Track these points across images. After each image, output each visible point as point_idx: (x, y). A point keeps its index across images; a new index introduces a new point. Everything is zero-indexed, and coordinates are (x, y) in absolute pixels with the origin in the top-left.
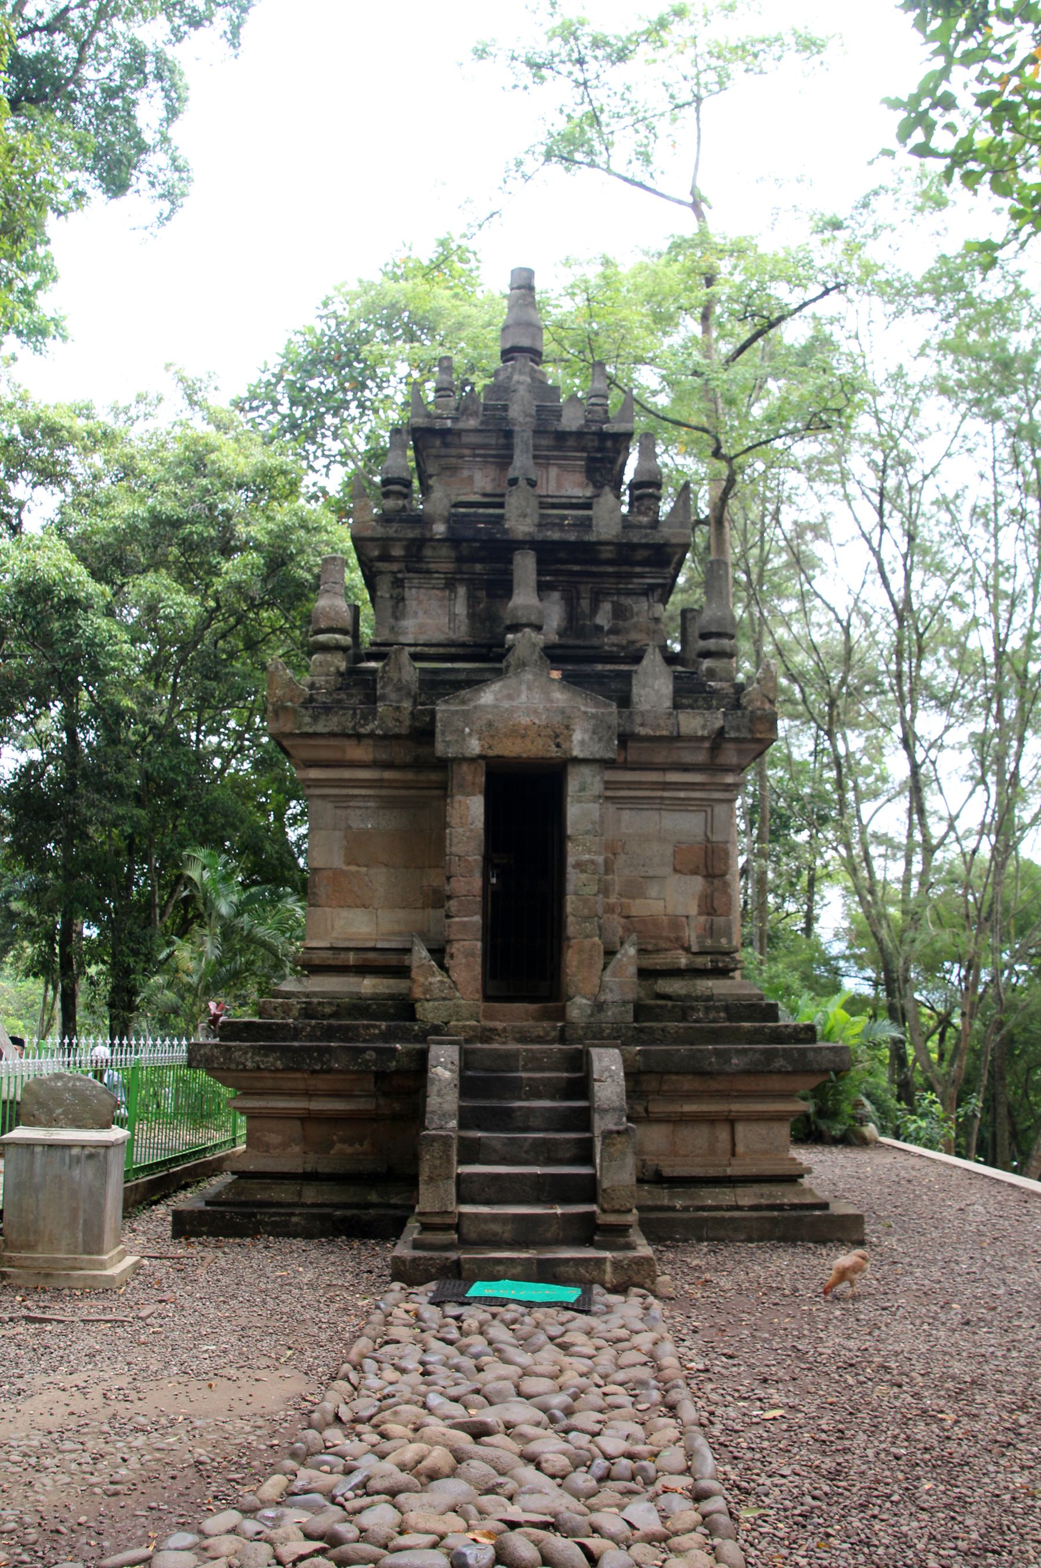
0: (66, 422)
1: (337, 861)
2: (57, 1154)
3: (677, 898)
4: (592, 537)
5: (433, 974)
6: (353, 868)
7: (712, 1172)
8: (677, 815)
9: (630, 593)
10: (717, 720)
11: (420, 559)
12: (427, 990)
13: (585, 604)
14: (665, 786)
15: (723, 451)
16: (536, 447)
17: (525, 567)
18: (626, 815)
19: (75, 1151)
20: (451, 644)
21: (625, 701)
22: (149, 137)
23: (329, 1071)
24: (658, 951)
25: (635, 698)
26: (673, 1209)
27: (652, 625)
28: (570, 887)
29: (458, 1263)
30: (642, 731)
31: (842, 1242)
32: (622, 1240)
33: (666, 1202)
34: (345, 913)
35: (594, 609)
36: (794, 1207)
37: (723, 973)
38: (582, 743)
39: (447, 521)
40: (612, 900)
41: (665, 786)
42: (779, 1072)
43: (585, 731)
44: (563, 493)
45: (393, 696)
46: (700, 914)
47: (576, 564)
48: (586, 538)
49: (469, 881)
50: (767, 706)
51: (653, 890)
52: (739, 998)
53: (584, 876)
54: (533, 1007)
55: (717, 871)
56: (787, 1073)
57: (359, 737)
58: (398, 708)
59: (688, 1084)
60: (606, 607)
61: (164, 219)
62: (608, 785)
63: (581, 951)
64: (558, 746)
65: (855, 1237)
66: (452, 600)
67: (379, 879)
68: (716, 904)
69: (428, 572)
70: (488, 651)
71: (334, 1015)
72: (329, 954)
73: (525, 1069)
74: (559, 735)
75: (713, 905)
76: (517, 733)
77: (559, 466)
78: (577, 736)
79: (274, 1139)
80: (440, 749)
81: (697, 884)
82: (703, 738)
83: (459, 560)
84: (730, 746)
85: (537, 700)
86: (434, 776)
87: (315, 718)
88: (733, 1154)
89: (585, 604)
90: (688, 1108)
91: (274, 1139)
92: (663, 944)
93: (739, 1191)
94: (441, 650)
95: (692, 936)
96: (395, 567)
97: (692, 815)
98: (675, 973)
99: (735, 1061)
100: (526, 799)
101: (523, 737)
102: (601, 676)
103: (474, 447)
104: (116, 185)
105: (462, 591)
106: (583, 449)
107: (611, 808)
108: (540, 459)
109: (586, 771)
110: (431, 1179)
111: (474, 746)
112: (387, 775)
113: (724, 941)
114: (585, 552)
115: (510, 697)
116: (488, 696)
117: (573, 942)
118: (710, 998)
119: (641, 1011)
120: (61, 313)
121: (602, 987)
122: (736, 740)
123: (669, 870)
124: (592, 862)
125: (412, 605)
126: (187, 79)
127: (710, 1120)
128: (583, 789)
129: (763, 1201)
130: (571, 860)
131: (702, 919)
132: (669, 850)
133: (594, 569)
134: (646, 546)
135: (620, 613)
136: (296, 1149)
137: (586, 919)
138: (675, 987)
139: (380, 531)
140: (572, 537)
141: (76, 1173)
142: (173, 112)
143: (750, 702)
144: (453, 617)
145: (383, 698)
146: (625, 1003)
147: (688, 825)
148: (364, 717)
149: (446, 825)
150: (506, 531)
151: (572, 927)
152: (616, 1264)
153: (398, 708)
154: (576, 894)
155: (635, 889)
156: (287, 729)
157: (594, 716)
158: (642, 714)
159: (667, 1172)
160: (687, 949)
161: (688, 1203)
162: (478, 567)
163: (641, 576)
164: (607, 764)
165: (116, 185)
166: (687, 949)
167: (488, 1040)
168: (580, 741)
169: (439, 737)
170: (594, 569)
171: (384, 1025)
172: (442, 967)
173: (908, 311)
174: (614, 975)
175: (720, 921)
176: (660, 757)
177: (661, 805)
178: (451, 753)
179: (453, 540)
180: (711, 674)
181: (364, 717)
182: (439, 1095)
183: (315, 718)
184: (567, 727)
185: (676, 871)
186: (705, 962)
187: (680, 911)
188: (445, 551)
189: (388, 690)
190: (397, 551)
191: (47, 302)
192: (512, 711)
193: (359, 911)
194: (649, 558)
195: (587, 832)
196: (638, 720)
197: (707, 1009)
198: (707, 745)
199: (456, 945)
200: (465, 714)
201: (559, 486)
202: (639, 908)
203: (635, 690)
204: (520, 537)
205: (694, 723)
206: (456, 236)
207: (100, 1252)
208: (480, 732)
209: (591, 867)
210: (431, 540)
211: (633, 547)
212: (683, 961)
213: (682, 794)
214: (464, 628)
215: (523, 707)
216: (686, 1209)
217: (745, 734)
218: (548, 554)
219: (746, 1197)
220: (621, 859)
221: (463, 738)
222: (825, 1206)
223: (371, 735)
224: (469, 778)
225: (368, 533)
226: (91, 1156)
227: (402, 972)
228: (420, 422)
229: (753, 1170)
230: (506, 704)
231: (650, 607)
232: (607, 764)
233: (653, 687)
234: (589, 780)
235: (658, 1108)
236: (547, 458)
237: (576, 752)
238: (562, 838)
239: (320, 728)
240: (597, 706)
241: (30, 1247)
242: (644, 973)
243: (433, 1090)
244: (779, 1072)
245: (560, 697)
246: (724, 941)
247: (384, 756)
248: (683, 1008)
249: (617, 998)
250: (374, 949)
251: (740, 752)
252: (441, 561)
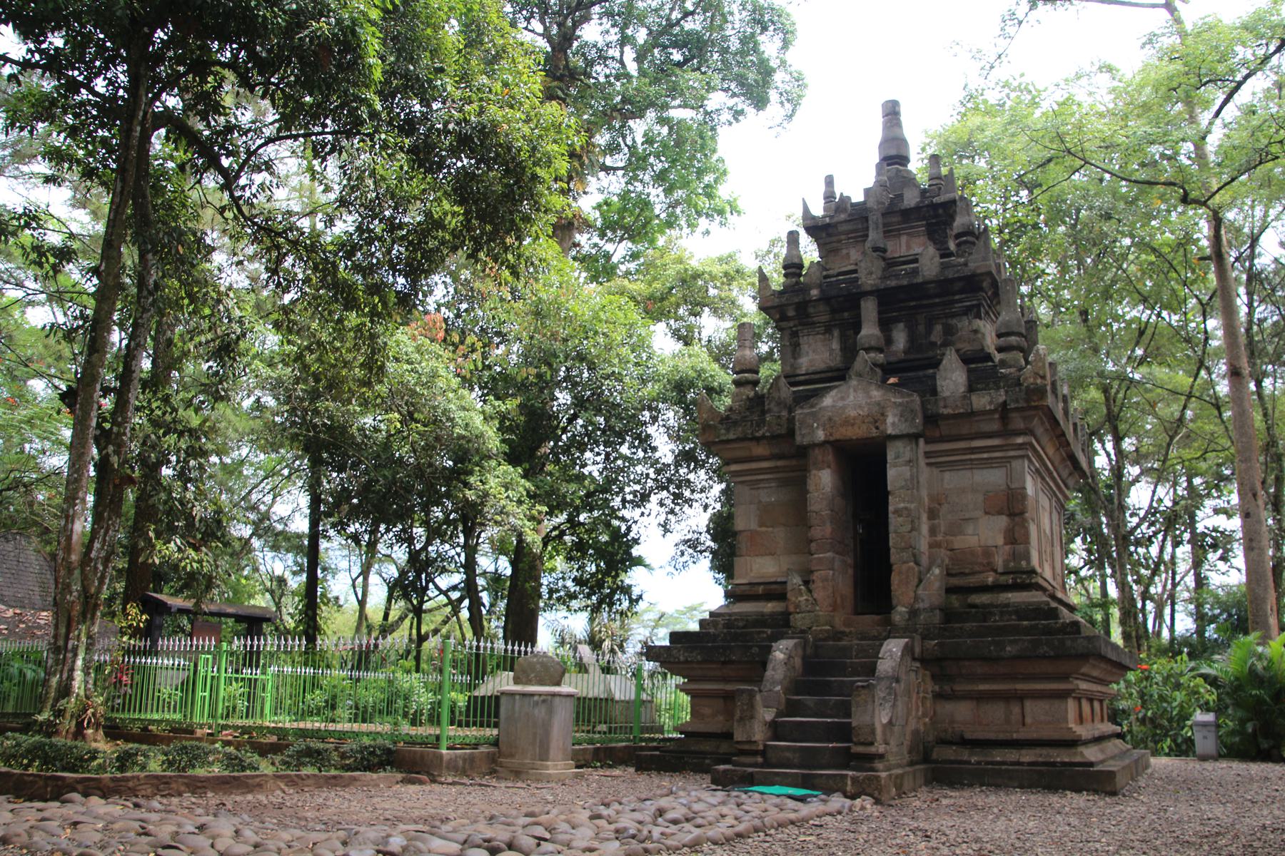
0: (707, 269)
1: (754, 525)
2: (527, 700)
3: (987, 533)
4: (920, 280)
5: (801, 595)
6: (764, 529)
7: (1001, 736)
8: (985, 471)
9: (954, 315)
10: (1001, 396)
11: (808, 316)
12: (797, 606)
13: (921, 328)
14: (1050, 474)
15: (1193, 195)
16: (885, 225)
17: (869, 309)
18: (947, 475)
19: (536, 698)
20: (830, 370)
21: (932, 390)
22: (774, 63)
23: (732, 662)
24: (973, 573)
25: (939, 389)
26: (969, 763)
27: (972, 336)
28: (891, 528)
29: (751, 774)
30: (946, 411)
31: (1096, 792)
32: (868, 765)
33: (965, 758)
34: (759, 560)
35: (929, 331)
36: (1064, 764)
38: (893, 424)
39: (820, 286)
40: (939, 538)
41: (1050, 474)
42: (1044, 657)
43: (895, 415)
44: (912, 252)
45: (776, 409)
46: (1006, 544)
48: (915, 281)
50: (1039, 381)
51: (970, 529)
52: (1030, 604)
53: (900, 519)
54: (876, 618)
55: (1017, 511)
56: (1050, 657)
57: (757, 440)
58: (779, 417)
59: (979, 668)
60: (938, 328)
61: (790, 117)
63: (900, 573)
64: (877, 428)
65: (1108, 789)
68: (1016, 535)
69: (814, 323)
71: (744, 627)
72: (747, 588)
73: (856, 657)
74: (877, 419)
75: (1016, 537)
76: (848, 422)
77: (908, 234)
78: (890, 420)
79: (707, 711)
81: (1003, 521)
82: (991, 412)
83: (833, 311)
84: (1014, 415)
87: (728, 430)
88: (1024, 724)
89: (921, 328)
90: (982, 687)
91: (707, 711)
92: (977, 568)
93: (1024, 752)
94: (823, 375)
95: (999, 562)
96: (791, 324)
97: (996, 471)
98: (985, 589)
99: (1008, 648)
100: (863, 465)
101: (853, 425)
103: (847, 233)
104: (760, 102)
105: (836, 333)
106: (924, 218)
107: (936, 471)
110: (741, 719)
111: (821, 435)
112: (780, 463)
113: (1024, 563)
115: (842, 399)
116: (828, 401)
117: (894, 567)
118: (1007, 605)
119: (949, 615)
120: (735, 196)
121: (916, 598)
122: (1017, 409)
123: (979, 513)
124: (906, 508)
125: (805, 347)
126: (794, 18)
127: (1007, 697)
128: (897, 457)
129: (1040, 759)
130: (891, 508)
131: (1007, 548)
132: (980, 498)
133: (925, 302)
134: (960, 279)
136: (721, 718)
137: (903, 549)
138: (984, 599)
140: (905, 282)
141: (536, 711)
142: (786, 44)
143: (1026, 379)
145: (769, 411)
146: (932, 609)
147: (994, 478)
148: (758, 425)
149: (807, 492)
150: (859, 286)
151: (894, 557)
152: (854, 780)
153: (779, 417)
154: (896, 532)
155: (956, 529)
156: (710, 439)
157: (900, 404)
158: (945, 399)
159: (968, 736)
160: (995, 571)
161: (982, 759)
162: (846, 314)
163: (960, 301)
165: (760, 102)
166: (995, 571)
167: (840, 639)
168: (892, 424)
169: (797, 433)
170: (925, 302)
171: (769, 631)
172: (810, 591)
174: (925, 589)
175: (1020, 548)
176: (965, 430)
178: (806, 441)
179: (825, 299)
181: (758, 425)
182: (774, 669)
183: (728, 430)
184: (883, 414)
185: (986, 513)
187: (990, 543)
188: (822, 307)
189: (772, 405)
190: (791, 313)
191: (723, 192)
192: (844, 408)
193: (768, 558)
195: (902, 487)
196: (942, 404)
197: (1002, 613)
198: (997, 416)
199: (816, 574)
200: (814, 415)
201: (909, 247)
202: (959, 542)
203: (938, 383)
204: (869, 289)
205: (981, 401)
206: (975, 83)
207: (547, 760)
208: (824, 425)
209: (905, 512)
210: (811, 301)
211: (952, 281)
213: (985, 456)
214: (838, 358)
216: (979, 763)
217: (1022, 404)
219: (1027, 756)
220: (945, 508)
221: (813, 430)
222: (1091, 764)
223: (763, 437)
224: (820, 457)
225: (769, 304)
226: (544, 701)
227: (782, 597)
229: (1035, 736)
230: (840, 404)
231: (970, 323)
232: (913, 438)
234: (901, 450)
235: (960, 687)
236: (899, 230)
239: (731, 436)
240: (902, 397)
241: (512, 756)
243: (770, 666)
244: (1044, 657)
245: (876, 394)
246: (1024, 563)
247: (776, 451)
248: (984, 612)
249: (927, 605)
250: (776, 583)
251: (1024, 418)
252: (821, 314)
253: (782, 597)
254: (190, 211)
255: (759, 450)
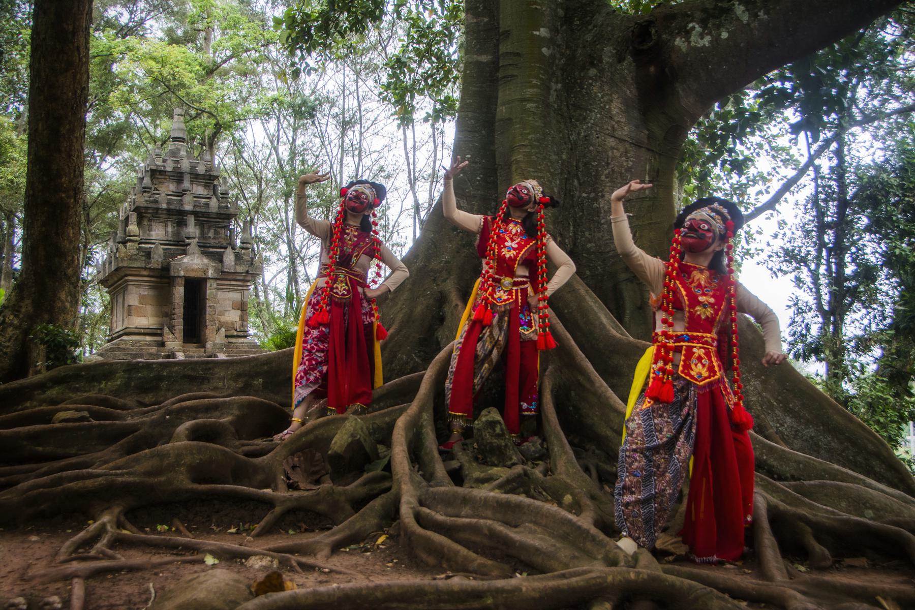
14: (231, 285)
37: (245, 337)
41: (231, 285)
47: (204, 218)
49: (179, 310)
51: (227, 314)
60: (212, 231)
62: (218, 284)
66: (166, 226)
67: (149, 309)
70: (179, 245)
80: (172, 274)
81: (239, 312)
85: (199, 261)
86: (166, 280)
89: (206, 230)
95: (237, 326)
100: (195, 288)
102: (212, 252)
108: (192, 182)
109: (212, 281)
111: (182, 274)
114: (207, 215)
125: (154, 227)
135: (216, 233)
139: (146, 205)
144: (166, 232)
147: (237, 296)
164: (217, 279)
168: (210, 273)
173: (792, 276)
176: (230, 277)
177: (230, 290)
180: (244, 254)
186: (241, 334)
194: (225, 216)
202: (222, 319)
212: (235, 333)
215: (194, 262)
218: (195, 214)
221: (179, 271)
228: (154, 168)
233: (229, 258)
237: (210, 276)
238: (205, 299)
242: (227, 337)
253: (161, 335)
254: (900, 135)
255: (145, 273)
